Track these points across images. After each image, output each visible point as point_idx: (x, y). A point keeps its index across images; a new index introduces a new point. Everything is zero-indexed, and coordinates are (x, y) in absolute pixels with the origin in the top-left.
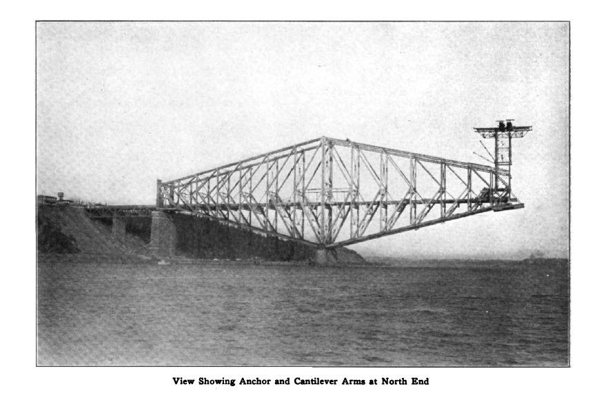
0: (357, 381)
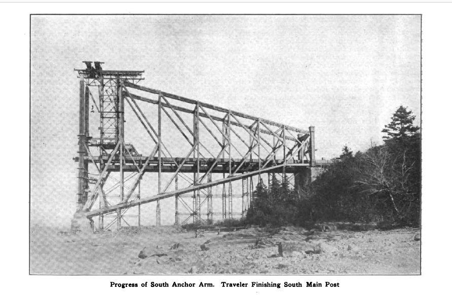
0: (210, 284)
